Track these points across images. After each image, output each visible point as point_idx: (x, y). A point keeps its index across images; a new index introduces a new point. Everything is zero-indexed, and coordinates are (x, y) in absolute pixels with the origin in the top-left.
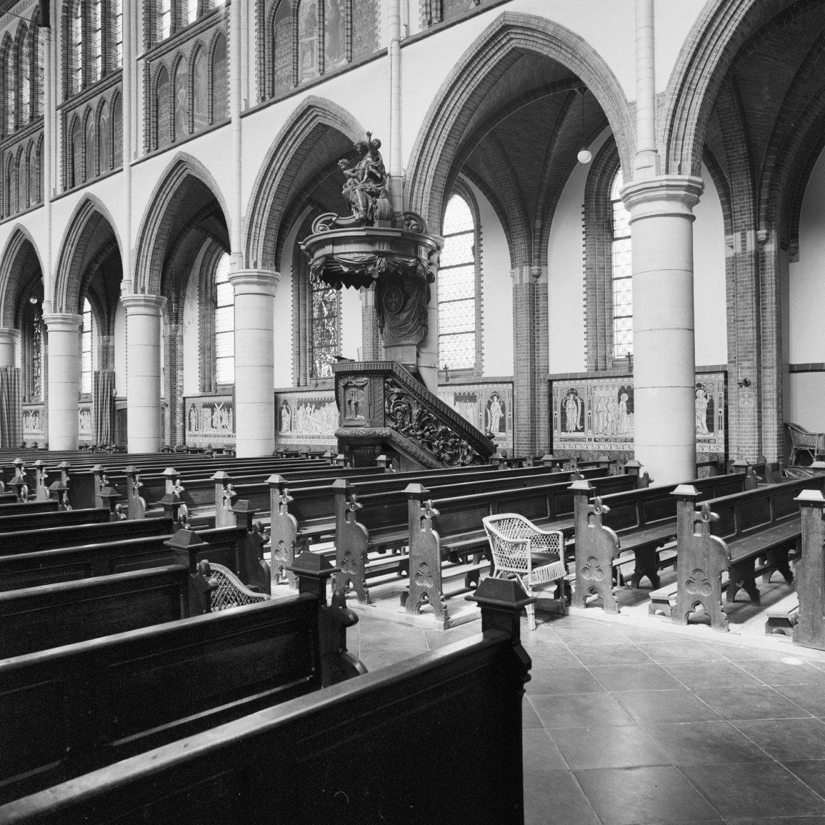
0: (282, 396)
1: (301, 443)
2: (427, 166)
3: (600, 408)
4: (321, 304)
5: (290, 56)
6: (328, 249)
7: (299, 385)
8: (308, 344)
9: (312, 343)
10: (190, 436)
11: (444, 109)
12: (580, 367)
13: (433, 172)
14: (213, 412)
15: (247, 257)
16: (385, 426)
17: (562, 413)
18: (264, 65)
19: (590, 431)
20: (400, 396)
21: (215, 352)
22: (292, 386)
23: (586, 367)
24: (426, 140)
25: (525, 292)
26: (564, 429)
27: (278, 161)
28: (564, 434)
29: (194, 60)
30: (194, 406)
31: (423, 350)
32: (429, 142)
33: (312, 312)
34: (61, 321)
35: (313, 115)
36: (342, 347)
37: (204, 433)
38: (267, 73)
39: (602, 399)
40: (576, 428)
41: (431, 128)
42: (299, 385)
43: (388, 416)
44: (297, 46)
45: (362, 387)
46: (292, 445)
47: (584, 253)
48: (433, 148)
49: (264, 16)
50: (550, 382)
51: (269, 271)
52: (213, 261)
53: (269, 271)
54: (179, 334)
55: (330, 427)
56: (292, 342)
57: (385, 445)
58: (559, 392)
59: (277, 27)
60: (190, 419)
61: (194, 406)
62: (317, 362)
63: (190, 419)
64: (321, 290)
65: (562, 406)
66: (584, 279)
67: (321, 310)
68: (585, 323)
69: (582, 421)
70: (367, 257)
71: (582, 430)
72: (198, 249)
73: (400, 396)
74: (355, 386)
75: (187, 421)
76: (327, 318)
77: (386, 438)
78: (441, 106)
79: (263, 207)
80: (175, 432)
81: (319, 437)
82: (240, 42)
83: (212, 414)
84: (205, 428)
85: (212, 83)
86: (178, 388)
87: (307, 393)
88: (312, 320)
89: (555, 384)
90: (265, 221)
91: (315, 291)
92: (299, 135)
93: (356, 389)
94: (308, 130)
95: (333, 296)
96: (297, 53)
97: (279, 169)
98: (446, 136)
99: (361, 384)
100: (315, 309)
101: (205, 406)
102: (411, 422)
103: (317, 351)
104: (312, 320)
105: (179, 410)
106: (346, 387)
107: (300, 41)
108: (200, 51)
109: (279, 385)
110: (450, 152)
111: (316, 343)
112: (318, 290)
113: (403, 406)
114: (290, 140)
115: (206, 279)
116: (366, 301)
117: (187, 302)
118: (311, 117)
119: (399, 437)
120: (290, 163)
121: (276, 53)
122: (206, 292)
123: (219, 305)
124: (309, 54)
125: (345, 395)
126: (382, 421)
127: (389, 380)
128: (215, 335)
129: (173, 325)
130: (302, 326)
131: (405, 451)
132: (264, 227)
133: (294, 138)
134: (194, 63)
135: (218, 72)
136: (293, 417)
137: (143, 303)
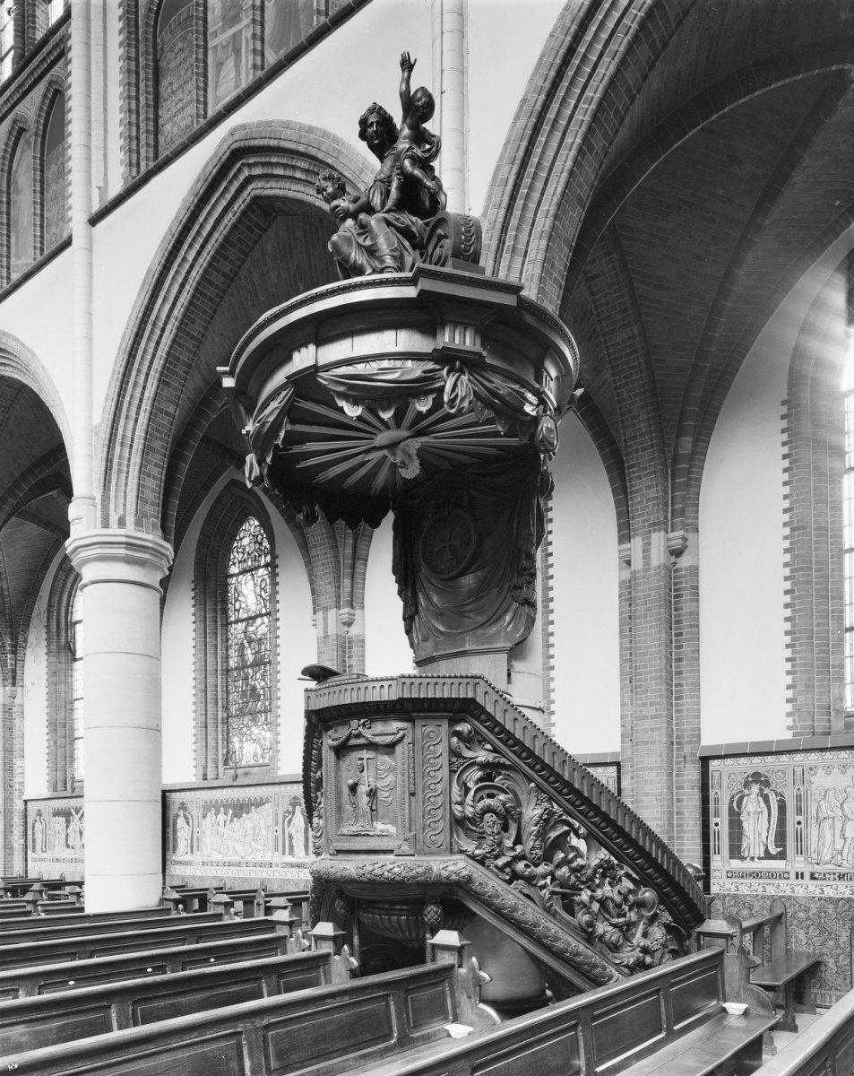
0: (176, 798)
1: (209, 874)
2: (532, 206)
3: (824, 812)
4: (242, 644)
5: (191, 86)
6: (303, 358)
7: (205, 779)
8: (220, 709)
9: (226, 708)
10: (34, 860)
11: (588, 37)
12: (777, 728)
13: (549, 222)
14: (68, 822)
15: (105, 507)
16: (452, 852)
17: (731, 822)
18: (138, 113)
19: (800, 858)
20: (490, 770)
21: (72, 730)
22: (194, 779)
23: (789, 728)
24: (536, 130)
25: (651, 589)
26: (736, 852)
27: (165, 299)
28: (736, 864)
29: (11, 161)
30: (39, 814)
31: (518, 666)
32: (542, 138)
33: (227, 657)
34: (122, 551)
35: (242, 178)
36: (279, 711)
37: (55, 856)
38: (142, 129)
39: (830, 793)
40: (767, 851)
41: (550, 95)
42: (205, 779)
43: (460, 823)
44: (206, 54)
45: (390, 748)
46: (194, 877)
47: (786, 497)
48: (550, 154)
49: (137, 15)
50: (705, 761)
51: (150, 537)
52: (69, 584)
53: (150, 537)
54: (17, 701)
55: (260, 848)
56: (194, 707)
57: (453, 901)
58: (725, 781)
59: (165, 36)
60: (33, 834)
61: (39, 814)
62: (235, 739)
63: (33, 834)
64: (242, 621)
65: (731, 809)
66: (786, 551)
67: (242, 656)
68: (788, 639)
69: (781, 838)
70: (414, 370)
71: (782, 856)
72: (45, 567)
73: (490, 770)
74: (371, 746)
75: (30, 837)
76: (250, 666)
77: (458, 884)
78: (577, 39)
79: (136, 402)
80: (11, 854)
81: (239, 864)
82: (89, 122)
83: (67, 827)
84: (57, 848)
85: (42, 193)
86: (17, 786)
87: (219, 791)
88: (227, 671)
89: (714, 764)
90: (140, 433)
91: (231, 623)
92: (210, 234)
93: (371, 754)
94: (239, 206)
95: (263, 629)
96: (206, 69)
97: (168, 317)
98: (587, 118)
99: (389, 739)
100: (232, 652)
101: (57, 813)
102: (518, 841)
103: (234, 723)
104: (227, 671)
105: (17, 820)
106: (341, 750)
107: (210, 45)
108: (22, 141)
109: (170, 778)
110: (590, 175)
111: (233, 709)
112: (237, 622)
113: (502, 797)
114: (191, 246)
115: (58, 615)
116: (326, 627)
117: (28, 651)
118: (236, 184)
119: (488, 882)
120: (191, 303)
121: (162, 90)
122: (58, 635)
123: (77, 657)
124: (230, 63)
125: (338, 769)
126: (443, 838)
127: (464, 728)
128: (72, 703)
129: (8, 688)
130: (211, 680)
131: (488, 904)
132: (138, 445)
133: (201, 241)
134: (10, 167)
135: (49, 174)
136: (196, 830)
137: (122, 551)
